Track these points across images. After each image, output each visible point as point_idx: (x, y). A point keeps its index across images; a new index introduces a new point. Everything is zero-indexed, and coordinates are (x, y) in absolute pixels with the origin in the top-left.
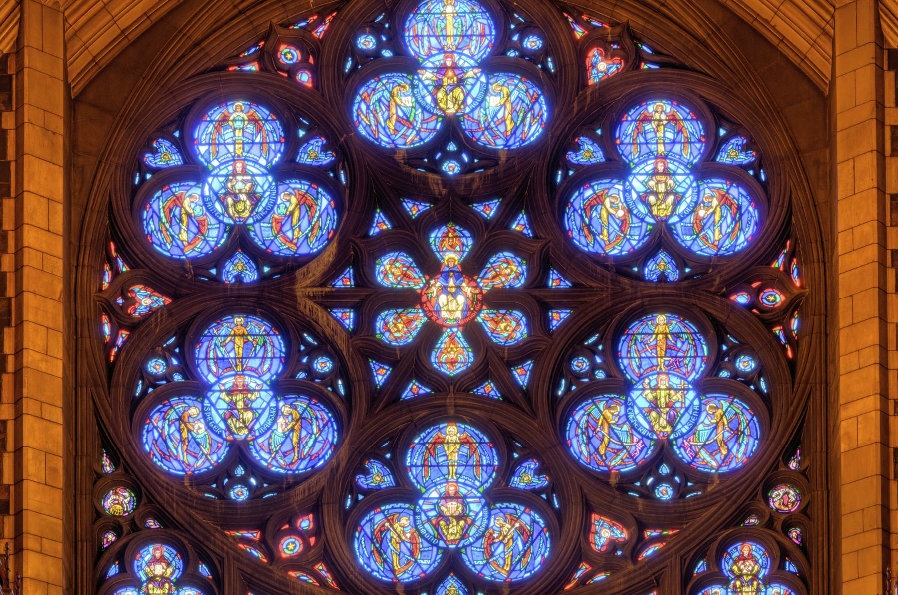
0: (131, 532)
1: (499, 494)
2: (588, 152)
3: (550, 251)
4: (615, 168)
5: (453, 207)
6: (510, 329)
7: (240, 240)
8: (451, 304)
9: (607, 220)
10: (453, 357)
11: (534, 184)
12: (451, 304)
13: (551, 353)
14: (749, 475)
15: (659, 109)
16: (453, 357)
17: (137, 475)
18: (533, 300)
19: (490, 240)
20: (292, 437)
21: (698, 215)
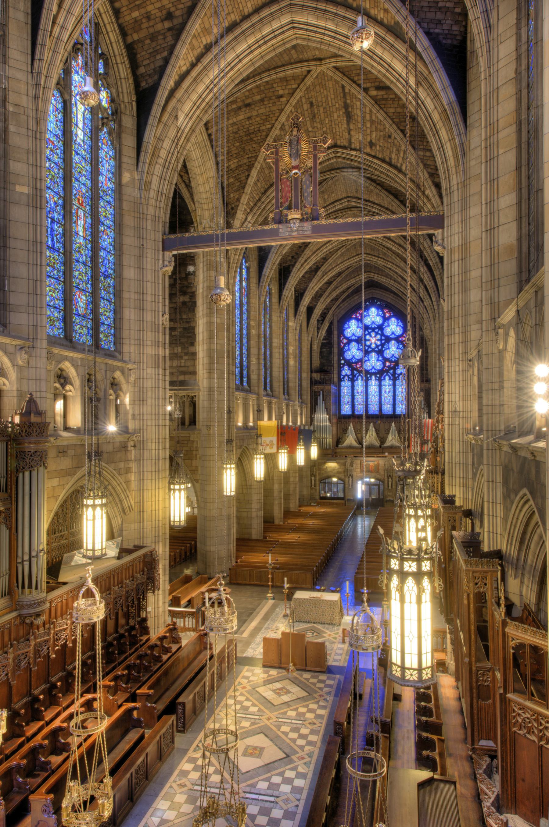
0: (344, 365)
1: (378, 360)
2: (386, 324)
3: (382, 334)
4: (389, 326)
5: (373, 329)
6: (379, 343)
7: (353, 334)
8: (373, 340)
9: (359, 332)
10: (373, 346)
11: (381, 327)
12: (373, 340)
13: (383, 345)
14: (473, 637)
15: (393, 319)
16: (373, 346)
17: (344, 359)
18: (381, 340)
19: (377, 333)
20: (358, 355)
21: (367, 671)
